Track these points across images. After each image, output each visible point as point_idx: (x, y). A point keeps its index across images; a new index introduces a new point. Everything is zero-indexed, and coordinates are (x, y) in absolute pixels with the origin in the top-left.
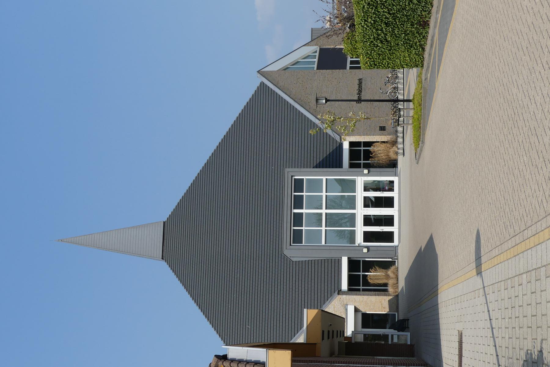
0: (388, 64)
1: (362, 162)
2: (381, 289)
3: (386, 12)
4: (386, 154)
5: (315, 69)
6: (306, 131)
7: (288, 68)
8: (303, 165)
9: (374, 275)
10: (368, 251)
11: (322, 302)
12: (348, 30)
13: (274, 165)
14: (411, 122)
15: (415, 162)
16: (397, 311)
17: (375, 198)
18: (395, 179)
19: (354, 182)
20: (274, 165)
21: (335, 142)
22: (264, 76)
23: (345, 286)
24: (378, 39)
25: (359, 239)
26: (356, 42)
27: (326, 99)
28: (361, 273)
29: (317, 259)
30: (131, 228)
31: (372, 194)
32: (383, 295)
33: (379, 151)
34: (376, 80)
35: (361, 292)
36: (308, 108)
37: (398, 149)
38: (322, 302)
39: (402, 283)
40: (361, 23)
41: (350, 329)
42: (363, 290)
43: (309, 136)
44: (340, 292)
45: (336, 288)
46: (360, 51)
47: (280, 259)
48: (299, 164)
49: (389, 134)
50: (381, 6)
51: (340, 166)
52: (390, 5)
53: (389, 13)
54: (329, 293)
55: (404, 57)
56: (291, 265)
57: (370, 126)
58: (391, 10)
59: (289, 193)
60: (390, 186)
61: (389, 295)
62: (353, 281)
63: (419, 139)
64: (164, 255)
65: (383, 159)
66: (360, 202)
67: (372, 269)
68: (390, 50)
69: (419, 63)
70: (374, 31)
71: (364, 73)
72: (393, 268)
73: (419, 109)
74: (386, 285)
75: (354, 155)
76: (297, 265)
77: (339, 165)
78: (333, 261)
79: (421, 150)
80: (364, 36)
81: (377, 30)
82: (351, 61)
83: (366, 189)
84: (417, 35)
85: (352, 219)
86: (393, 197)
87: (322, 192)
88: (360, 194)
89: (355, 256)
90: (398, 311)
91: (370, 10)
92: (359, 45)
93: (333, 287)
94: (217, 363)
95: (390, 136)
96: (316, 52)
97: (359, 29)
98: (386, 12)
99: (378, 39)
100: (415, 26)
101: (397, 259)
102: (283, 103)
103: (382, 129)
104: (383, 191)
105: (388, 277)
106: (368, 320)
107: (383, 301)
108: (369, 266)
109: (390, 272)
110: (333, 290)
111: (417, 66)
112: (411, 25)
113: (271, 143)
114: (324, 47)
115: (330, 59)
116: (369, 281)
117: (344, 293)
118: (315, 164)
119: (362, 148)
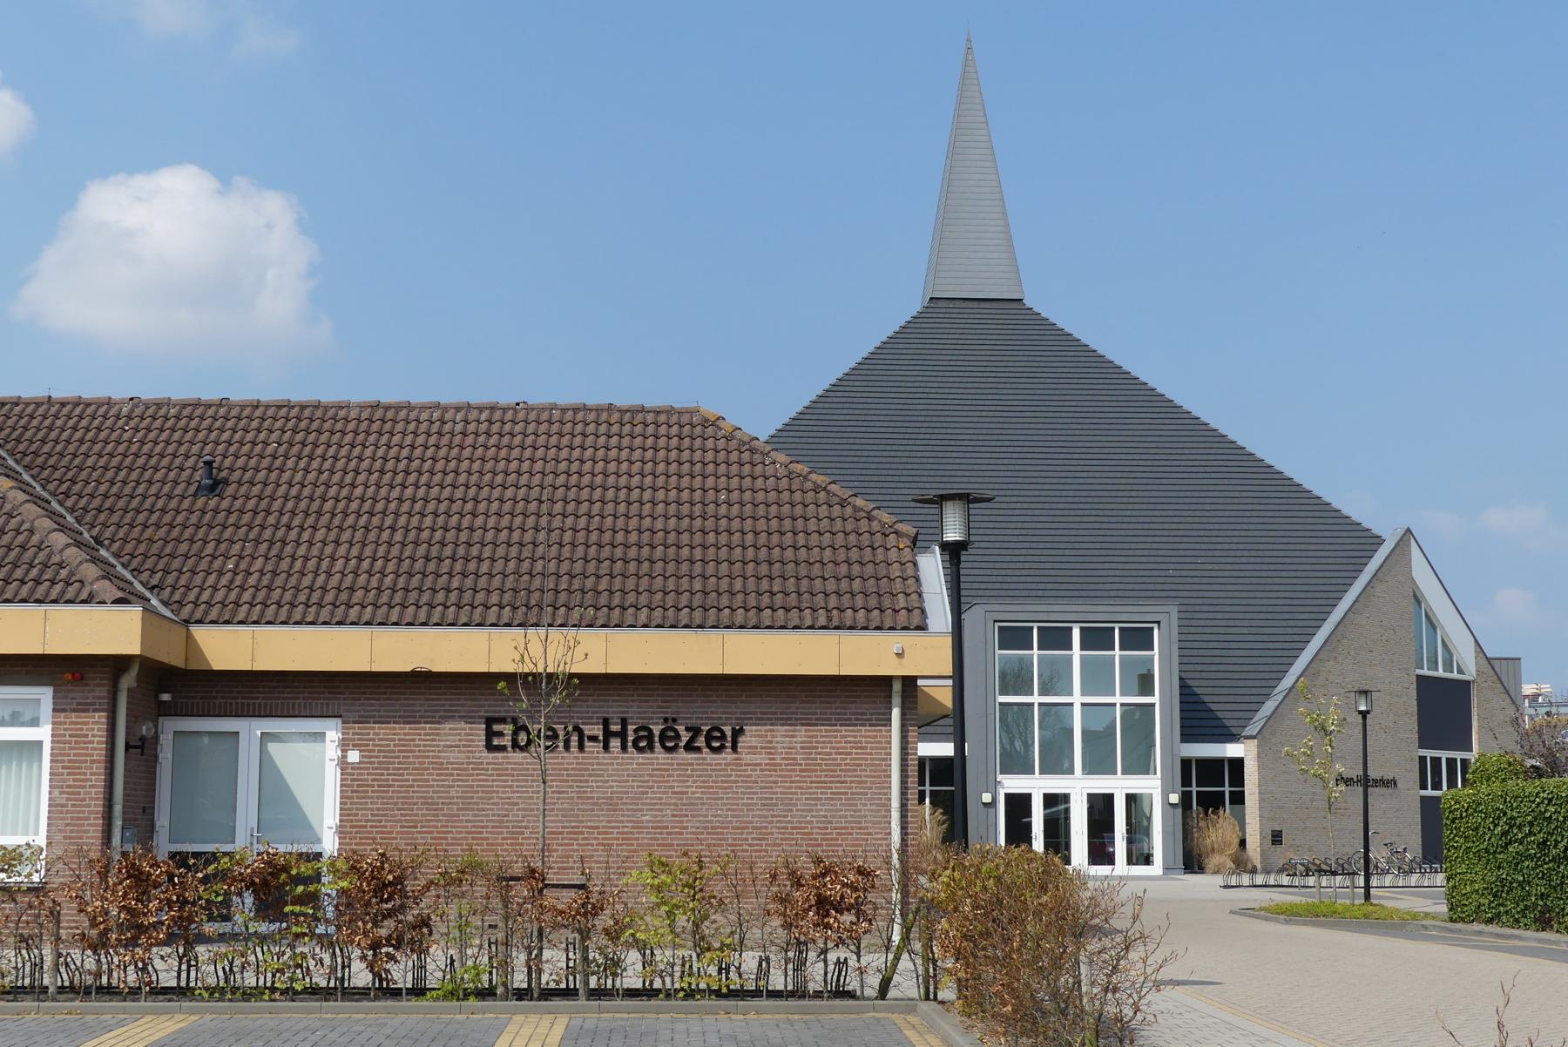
5: (1419, 672)
7: (1419, 602)
10: (985, 804)
12: (1529, 762)
15: (1235, 908)
18: (1157, 868)
21: (1241, 723)
22: (1397, 545)
25: (1013, 784)
26: (1504, 780)
30: (1006, 220)
33: (1219, 831)
34: (1398, 820)
49: (1263, 853)
55: (1473, 882)
59: (1119, 615)
63: (1290, 914)
64: (941, 304)
68: (1487, 851)
69: (1461, 911)
71: (1411, 794)
75: (1211, 770)
77: (1188, 735)
79: (1267, 919)
81: (1531, 824)
82: (1439, 759)
84: (1522, 906)
85: (1056, 762)
88: (1119, 785)
92: (1496, 786)
96: (1460, 671)
97: (1532, 787)
99: (1511, 827)
103: (1277, 838)
113: (1223, 559)
115: (1443, 708)
118: (1191, 683)
119: (1227, 789)
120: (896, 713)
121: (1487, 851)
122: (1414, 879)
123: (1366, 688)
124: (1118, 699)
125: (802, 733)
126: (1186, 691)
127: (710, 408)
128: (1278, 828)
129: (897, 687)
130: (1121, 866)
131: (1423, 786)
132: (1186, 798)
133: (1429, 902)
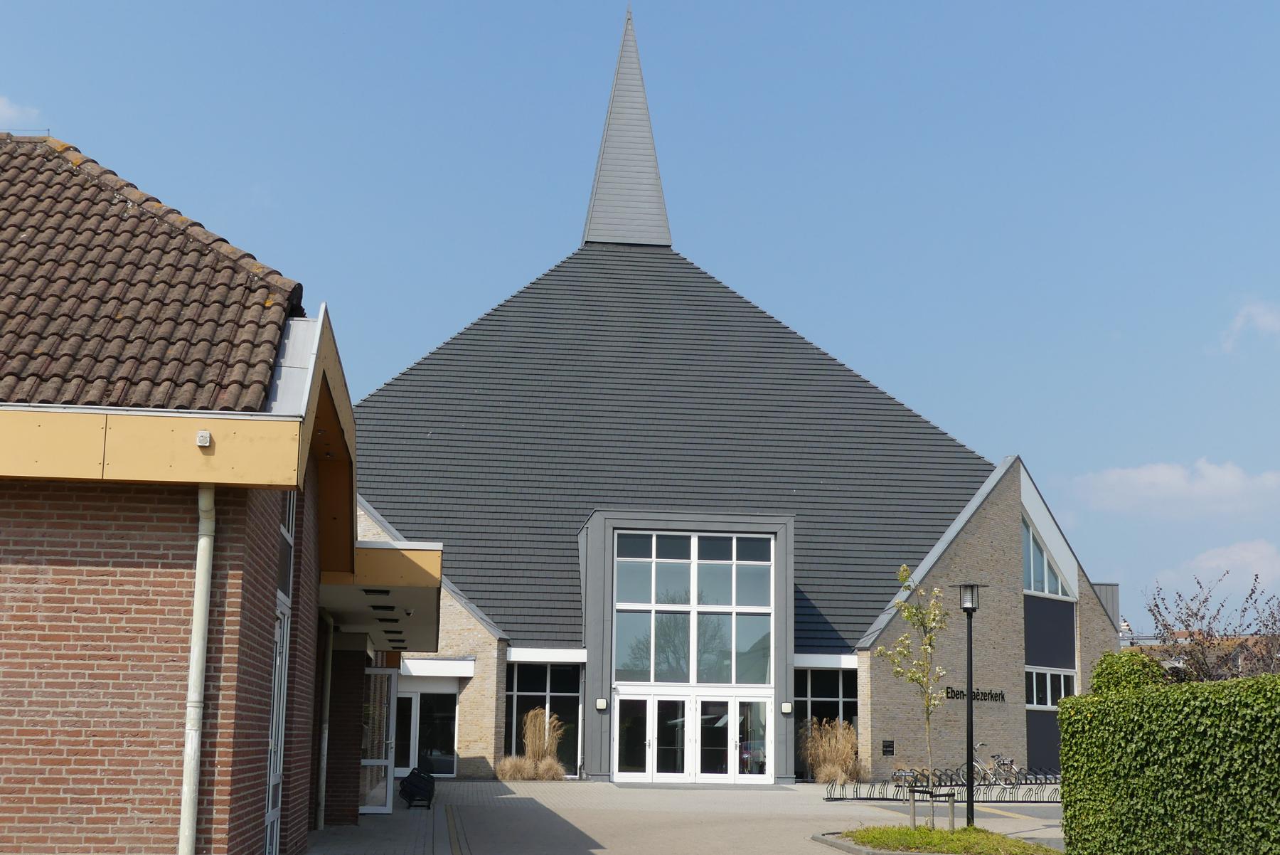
0: (1076, 769)
1: (809, 699)
2: (512, 739)
3: (1231, 766)
4: (828, 756)
5: (1026, 592)
6: (904, 556)
7: (1027, 527)
8: (801, 559)
9: (543, 723)
10: (600, 711)
11: (482, 603)
12: (1167, 665)
13: (801, 493)
14: (921, 821)
16: (460, 778)
17: (724, 730)
18: (768, 777)
19: (761, 678)
20: (801, 493)
21: (856, 635)
22: (1008, 470)
23: (519, 654)
24: (1149, 744)
26: (1137, 685)
27: (974, 610)
28: (548, 694)
29: (583, 591)
31: (733, 721)
32: (496, 744)
34: (1004, 732)
35: (504, 694)
36: (934, 572)
37: (843, 786)
38: (482, 603)
39: (521, 790)
40: (1195, 698)
41: (416, 665)
42: (509, 699)
43: (896, 562)
44: (505, 644)
45: (514, 635)
46: (1113, 695)
47: (583, 505)
48: (804, 553)
49: (874, 763)
50: (1249, 753)
51: (801, 647)
52: (1253, 776)
53: (1227, 775)
54: (505, 619)
56: (568, 532)
57: (894, 718)
58: (1238, 781)
60: (752, 765)
61: (496, 759)
62: (530, 675)
65: (817, 749)
66: (715, 693)
67: (559, 719)
68: (1116, 773)
70: (1175, 733)
71: (1018, 707)
72: (560, 769)
73: (954, 845)
74: (521, 751)
75: (826, 680)
76: (568, 545)
77: (803, 645)
78: (577, 629)
80: (1157, 705)
81: (1177, 741)
82: (1045, 675)
83: (744, 707)
84: (1162, 847)
86: (725, 771)
87: (738, 604)
88: (733, 694)
89: (588, 681)
90: (459, 778)
91: (1239, 723)
92: (1128, 693)
93: (516, 627)
94: (280, 290)
95: (869, 766)
96: (1064, 593)
97: (1177, 692)
98: (1231, 766)
99: (1149, 744)
100: (1189, 844)
101: (581, 779)
102: (945, 516)
103: (888, 748)
104: (741, 747)
105: (540, 756)
106: (440, 707)
107: (482, 745)
108: (566, 712)
109: (549, 762)
110: (509, 627)
111: (1068, 844)
112: (1192, 833)
113: (848, 485)
114: (1077, 614)
115: (1049, 627)
116: (531, 713)
117: (502, 654)
118: (802, 588)
119: (841, 700)
120: (204, 546)
121: (1116, 773)
122: (1021, 793)
123: (972, 583)
124: (734, 608)
125: (48, 575)
126: (799, 596)
127: (59, 138)
128: (889, 739)
129: (205, 502)
130: (733, 772)
131: (1030, 701)
132: (799, 710)
133: (1040, 822)
